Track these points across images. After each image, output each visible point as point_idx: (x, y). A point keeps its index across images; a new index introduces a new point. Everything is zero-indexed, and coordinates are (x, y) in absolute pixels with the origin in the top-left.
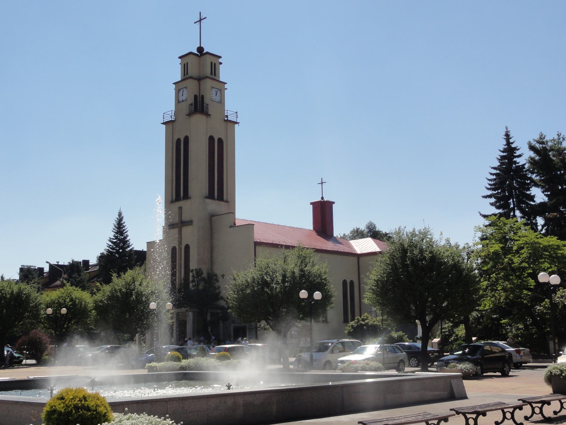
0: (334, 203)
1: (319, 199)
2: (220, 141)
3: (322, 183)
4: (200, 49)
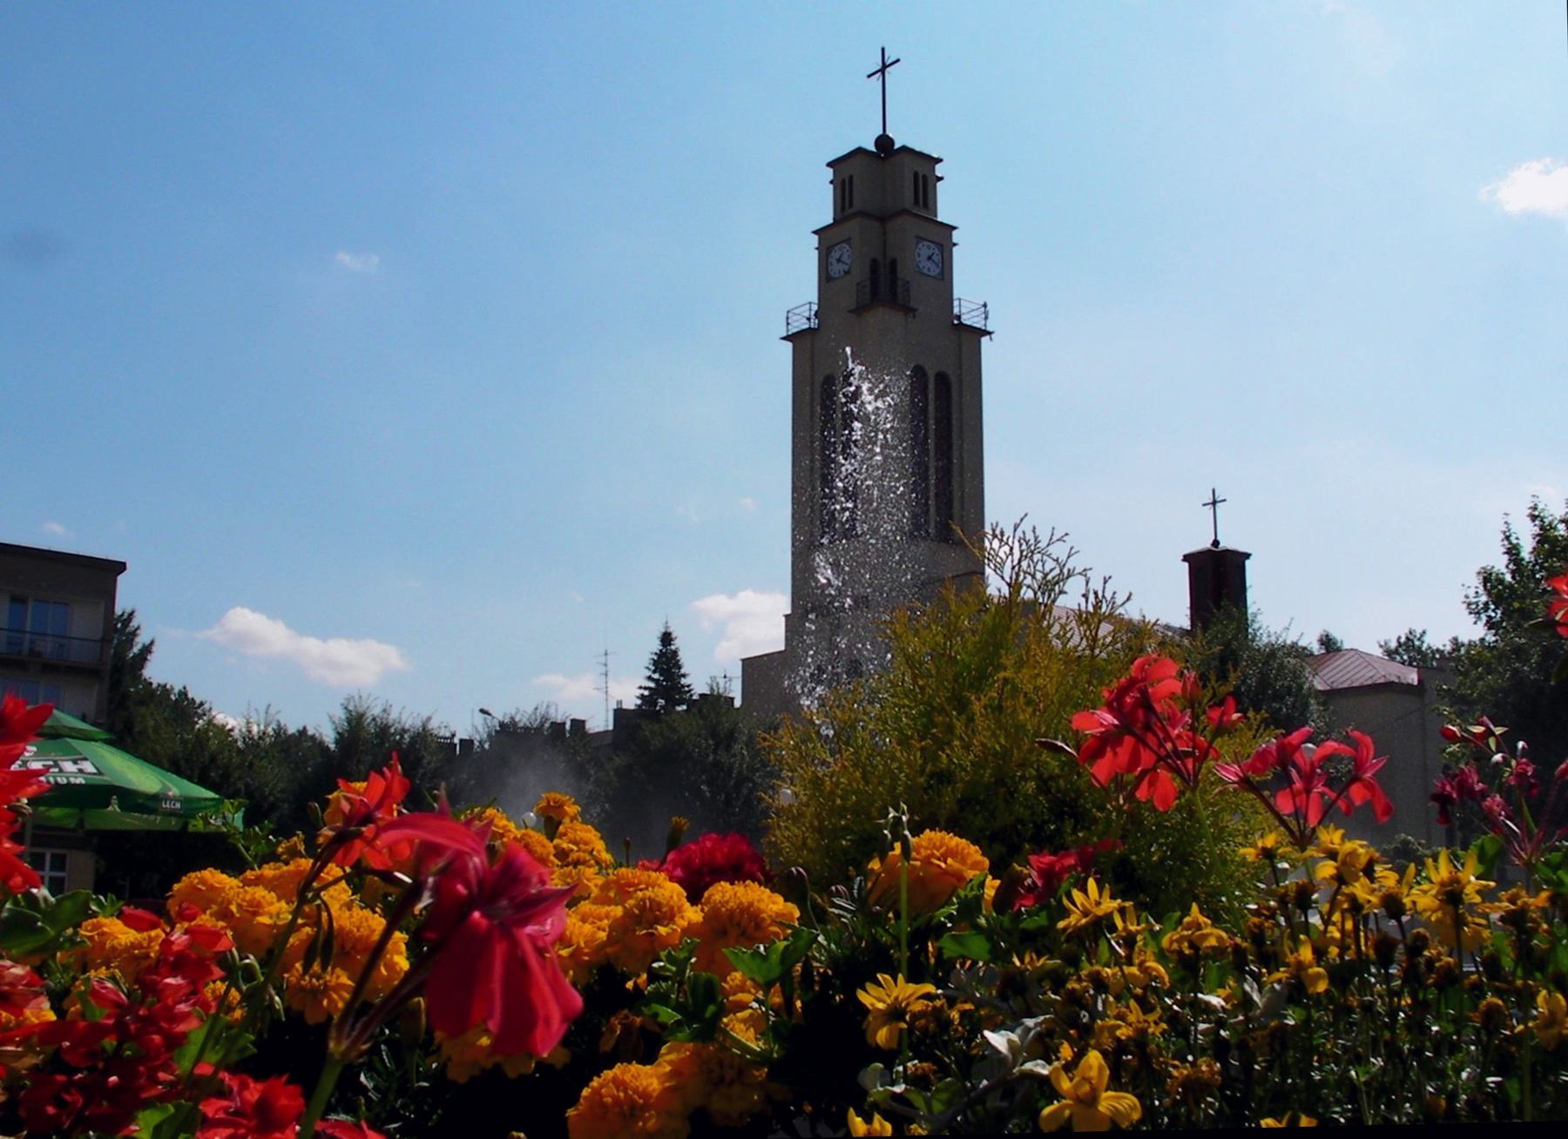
0: (1248, 556)
1: (1206, 544)
2: (943, 380)
3: (1214, 503)
4: (884, 142)
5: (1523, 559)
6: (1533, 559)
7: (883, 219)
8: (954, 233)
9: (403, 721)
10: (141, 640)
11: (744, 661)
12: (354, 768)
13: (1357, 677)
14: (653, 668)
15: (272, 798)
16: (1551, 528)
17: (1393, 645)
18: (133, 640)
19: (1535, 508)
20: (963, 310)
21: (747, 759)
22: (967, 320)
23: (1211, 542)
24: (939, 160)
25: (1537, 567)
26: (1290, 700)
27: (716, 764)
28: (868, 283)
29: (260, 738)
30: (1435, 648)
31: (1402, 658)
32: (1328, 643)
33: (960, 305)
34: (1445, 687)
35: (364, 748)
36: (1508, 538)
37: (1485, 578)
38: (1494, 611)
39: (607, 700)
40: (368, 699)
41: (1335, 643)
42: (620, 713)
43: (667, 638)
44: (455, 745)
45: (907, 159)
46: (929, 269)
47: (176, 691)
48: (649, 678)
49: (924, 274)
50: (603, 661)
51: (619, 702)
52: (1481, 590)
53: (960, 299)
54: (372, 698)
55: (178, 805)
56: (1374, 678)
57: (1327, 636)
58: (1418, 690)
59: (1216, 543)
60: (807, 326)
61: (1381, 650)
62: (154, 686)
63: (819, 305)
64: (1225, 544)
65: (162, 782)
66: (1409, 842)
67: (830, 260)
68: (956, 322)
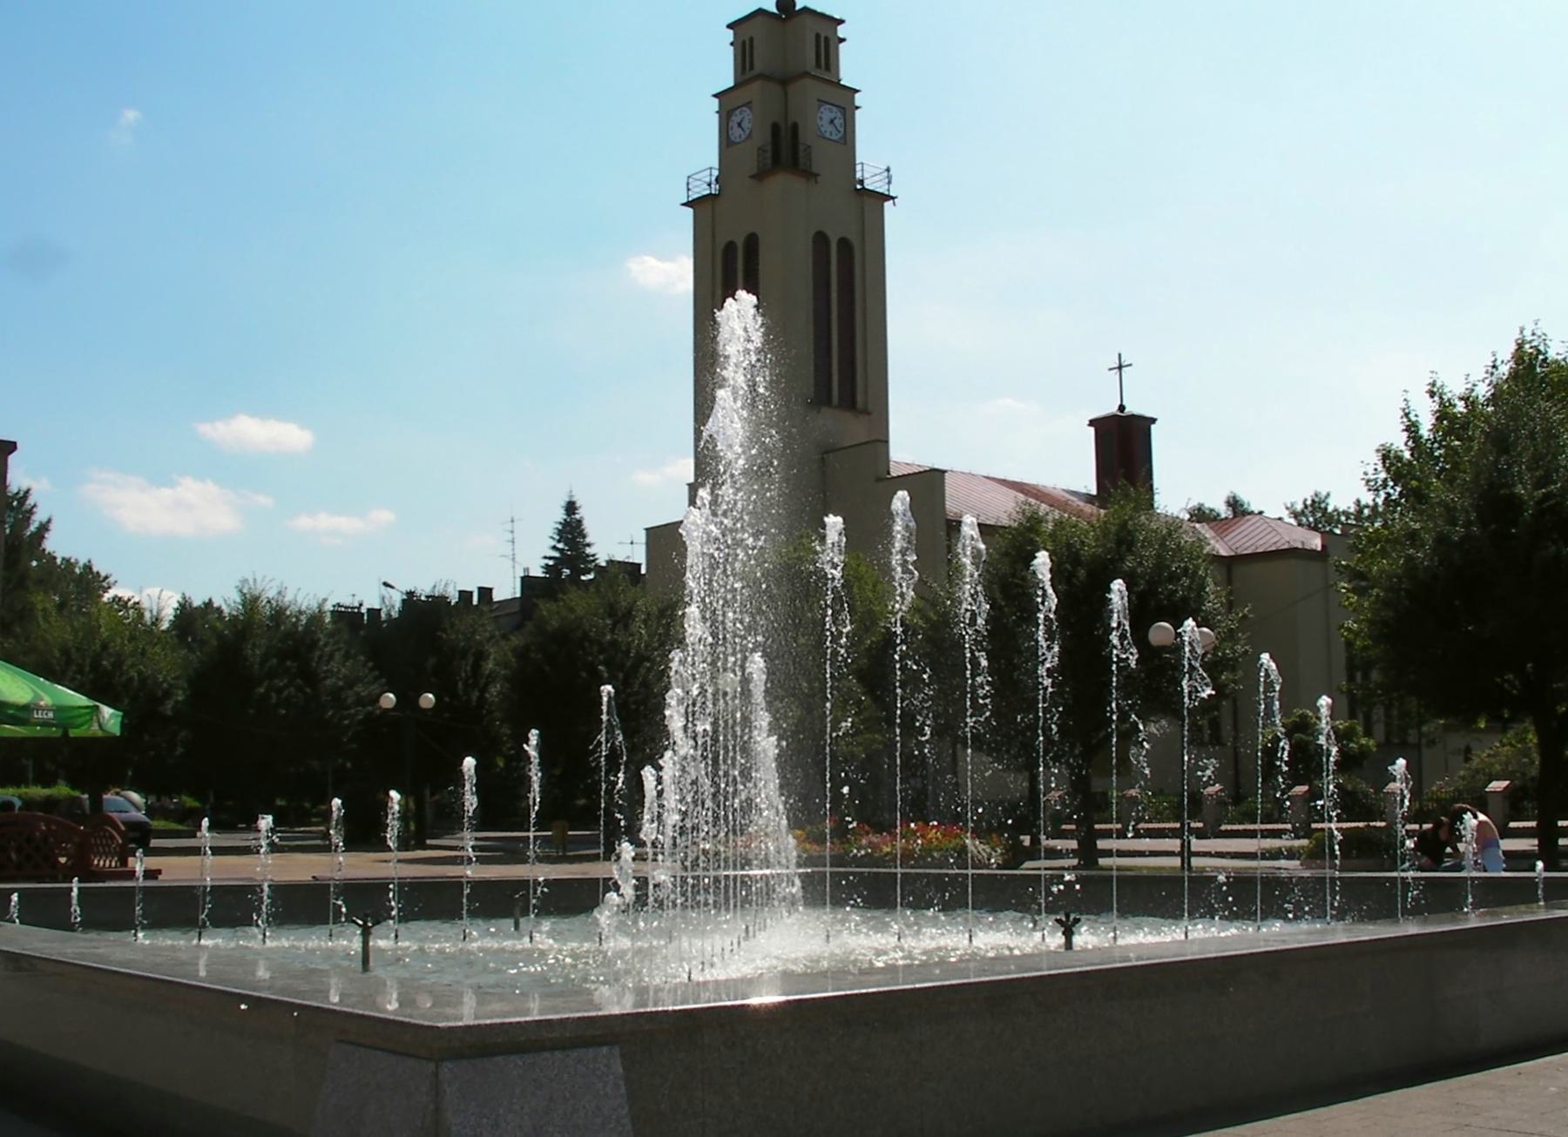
0: (1153, 420)
3: (1120, 367)
5: (1421, 437)
6: (1432, 437)
7: (784, 82)
8: (857, 95)
9: (299, 600)
10: (39, 517)
11: (647, 529)
12: (250, 652)
13: (1261, 542)
14: (557, 537)
15: (165, 685)
16: (1450, 404)
17: (1299, 507)
18: (29, 518)
19: (1433, 384)
20: (866, 175)
21: (646, 638)
22: (869, 185)
23: (1117, 408)
24: (841, 22)
25: (1436, 445)
26: (1186, 581)
27: (614, 643)
28: (769, 148)
29: (153, 624)
30: (1341, 510)
31: (1308, 520)
32: (1234, 504)
33: (862, 170)
34: (1343, 563)
35: (259, 632)
36: (1407, 415)
37: (1383, 455)
38: (1392, 488)
39: (514, 567)
40: (263, 581)
41: (1242, 505)
42: (527, 581)
43: (571, 508)
44: (363, 614)
45: (808, 20)
46: (831, 134)
47: (81, 564)
48: (554, 548)
49: (824, 138)
50: (510, 529)
51: (526, 570)
52: (1380, 467)
53: (862, 164)
54: (267, 579)
55: (51, 715)
56: (1279, 544)
57: (1234, 497)
58: (1320, 556)
59: (1122, 408)
60: (708, 192)
61: (1287, 512)
62: (59, 561)
63: (720, 170)
64: (1132, 408)
65: (34, 691)
66: (1307, 716)
67: (731, 124)
68: (859, 187)
